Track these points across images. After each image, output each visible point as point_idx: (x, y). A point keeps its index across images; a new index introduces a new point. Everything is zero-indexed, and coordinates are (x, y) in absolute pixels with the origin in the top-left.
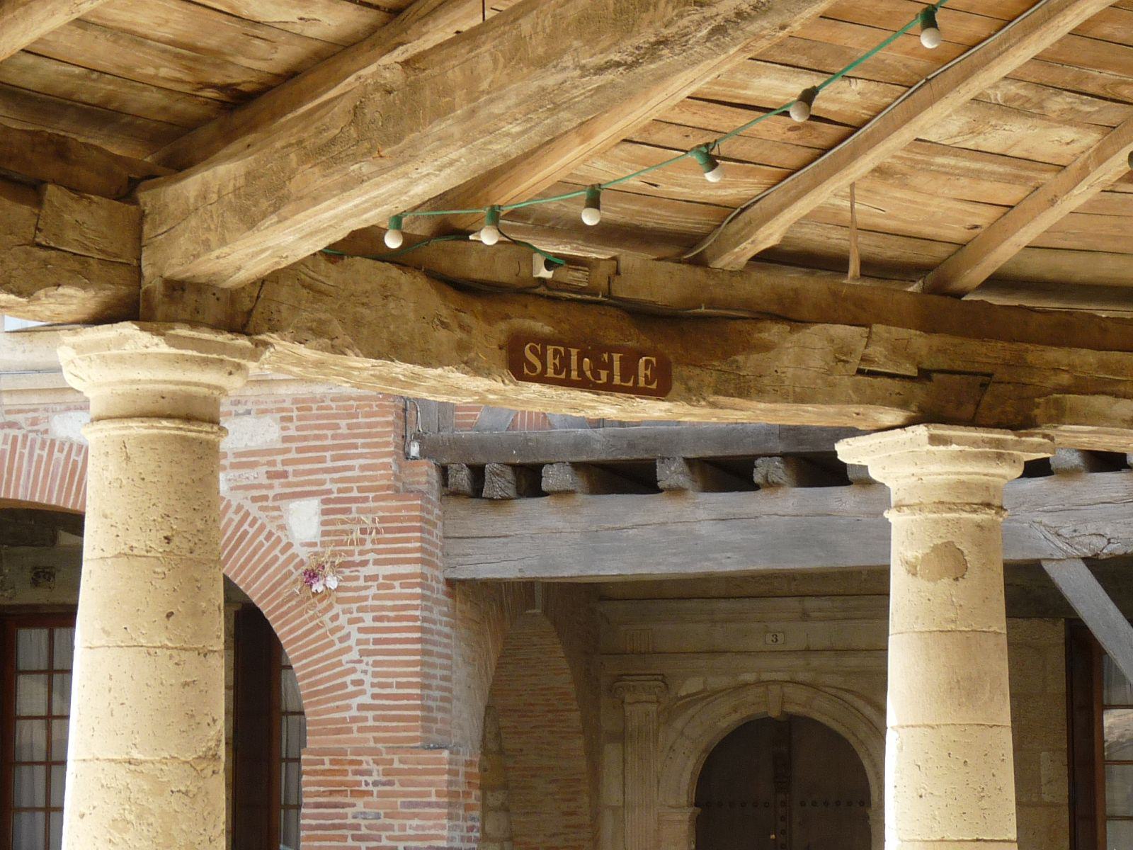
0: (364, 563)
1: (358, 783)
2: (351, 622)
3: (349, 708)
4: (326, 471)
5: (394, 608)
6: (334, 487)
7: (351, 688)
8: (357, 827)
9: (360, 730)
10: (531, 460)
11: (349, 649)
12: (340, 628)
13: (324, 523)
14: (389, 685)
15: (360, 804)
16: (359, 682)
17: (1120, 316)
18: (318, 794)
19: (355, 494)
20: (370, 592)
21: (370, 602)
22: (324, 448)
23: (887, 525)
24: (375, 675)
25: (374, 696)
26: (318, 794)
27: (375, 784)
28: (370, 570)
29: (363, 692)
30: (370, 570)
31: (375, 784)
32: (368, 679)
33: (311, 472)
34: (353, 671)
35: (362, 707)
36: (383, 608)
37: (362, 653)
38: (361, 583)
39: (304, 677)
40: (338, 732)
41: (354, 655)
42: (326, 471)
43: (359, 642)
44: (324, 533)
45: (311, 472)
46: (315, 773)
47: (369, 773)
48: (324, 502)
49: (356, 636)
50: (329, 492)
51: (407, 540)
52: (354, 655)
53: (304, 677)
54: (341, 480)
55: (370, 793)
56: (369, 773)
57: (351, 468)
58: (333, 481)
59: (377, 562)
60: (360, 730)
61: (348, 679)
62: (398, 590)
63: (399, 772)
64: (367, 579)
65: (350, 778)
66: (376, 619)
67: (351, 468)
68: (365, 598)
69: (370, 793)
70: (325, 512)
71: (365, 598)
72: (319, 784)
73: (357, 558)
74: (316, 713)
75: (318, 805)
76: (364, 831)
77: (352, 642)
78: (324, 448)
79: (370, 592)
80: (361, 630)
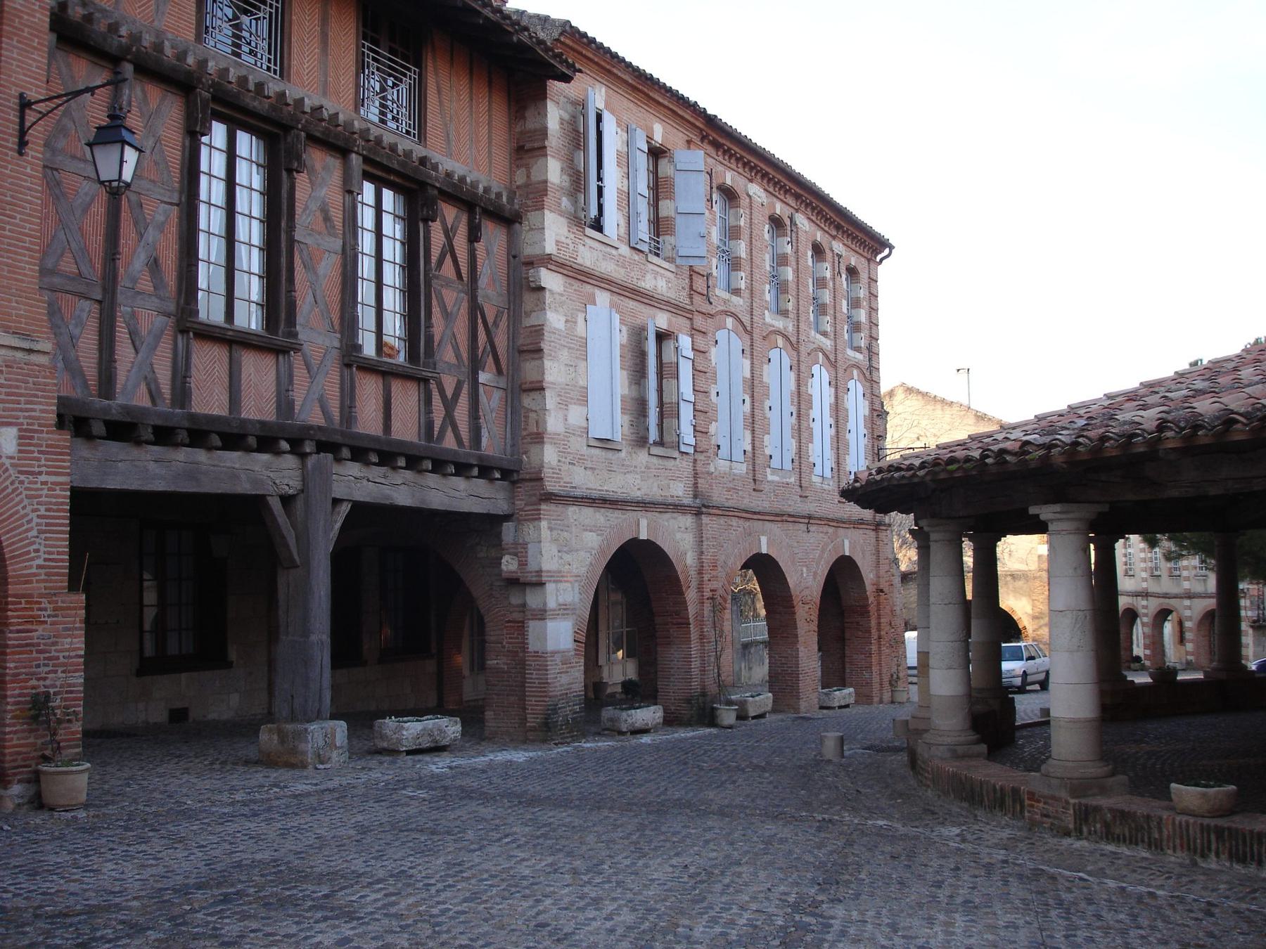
0: (40, 473)
1: (39, 616)
2: (34, 511)
3: (31, 567)
4: (21, 410)
5: (56, 504)
6: (25, 421)
7: (33, 555)
8: (39, 645)
9: (38, 581)
10: (84, 415)
11: (31, 529)
12: (26, 515)
13: (19, 445)
14: (52, 553)
15: (40, 628)
16: (37, 551)
17: (814, 626)
18: (19, 624)
19: (36, 427)
20: (45, 492)
21: (43, 499)
22: (21, 395)
23: (908, 513)
24: (46, 546)
25: (46, 560)
26: (19, 624)
27: (49, 616)
28: (43, 478)
29: (38, 557)
30: (43, 478)
31: (49, 616)
32: (42, 549)
33: (13, 410)
34: (33, 543)
35: (39, 567)
36: (50, 503)
37: (40, 532)
38: (38, 486)
39: (8, 546)
40: (27, 582)
41: (34, 533)
42: (21, 410)
43: (38, 524)
44: (20, 451)
45: (13, 410)
46: (16, 610)
47: (45, 609)
48: (20, 430)
49: (36, 520)
50: (22, 424)
51: (64, 461)
52: (34, 533)
53: (8, 546)
54: (29, 417)
55: (45, 622)
56: (45, 609)
57: (33, 410)
58: (25, 418)
59: (48, 473)
60: (38, 581)
61: (32, 548)
62: (58, 492)
63: (62, 609)
64: (42, 483)
65: (36, 613)
66: (47, 510)
67: (33, 410)
68: (41, 496)
69: (45, 622)
70: (20, 437)
71: (41, 496)
72: (18, 617)
73: (36, 469)
74: (14, 570)
75: (19, 631)
76: (42, 647)
77: (33, 524)
78: (21, 395)
79: (45, 492)
80: (38, 517)
